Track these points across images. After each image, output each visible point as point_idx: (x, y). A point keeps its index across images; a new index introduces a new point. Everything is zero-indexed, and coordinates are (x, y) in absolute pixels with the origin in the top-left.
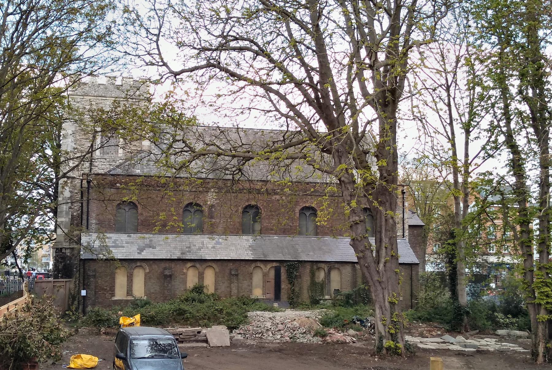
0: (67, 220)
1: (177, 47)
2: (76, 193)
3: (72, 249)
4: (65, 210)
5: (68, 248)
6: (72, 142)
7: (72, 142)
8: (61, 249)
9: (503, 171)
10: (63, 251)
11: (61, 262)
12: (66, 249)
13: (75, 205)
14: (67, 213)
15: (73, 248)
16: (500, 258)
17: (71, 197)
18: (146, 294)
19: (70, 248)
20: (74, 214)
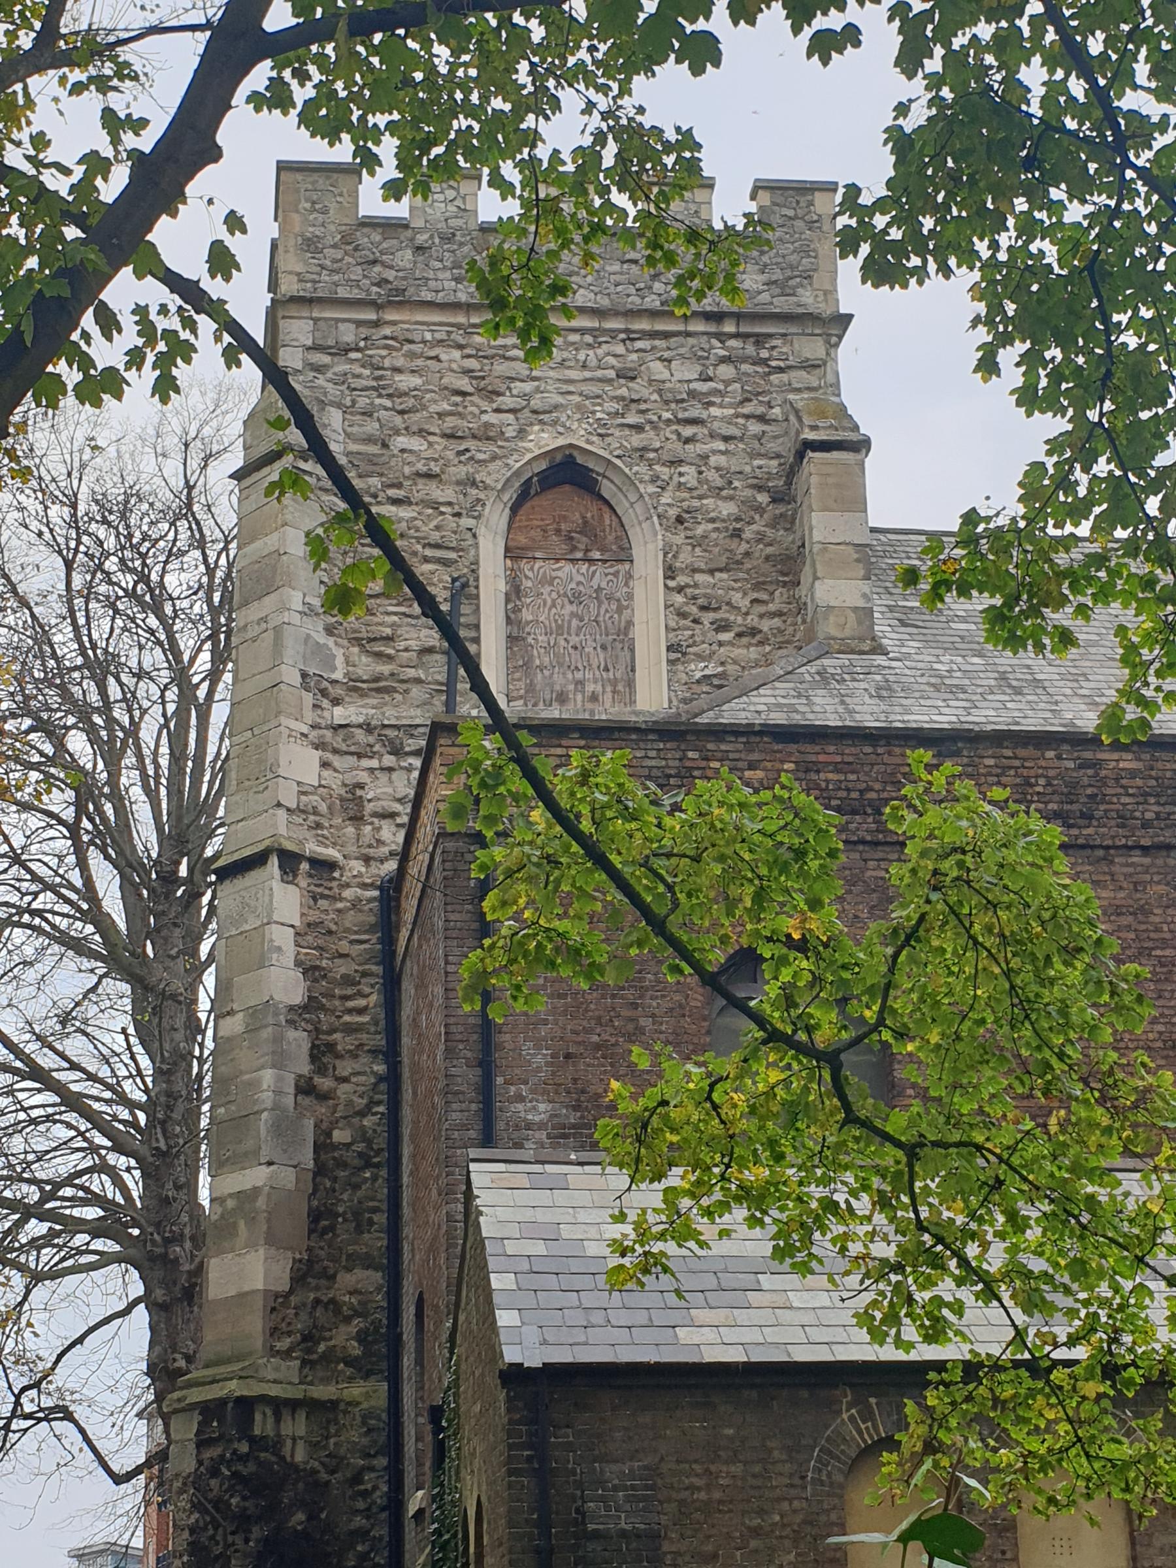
0: (287, 1178)
1: (556, 118)
2: (347, 980)
3: (324, 1412)
4: (267, 1098)
5: (294, 1405)
6: (308, 612)
7: (308, 612)
8: (245, 1405)
9: (1108, 468)
10: (262, 1424)
11: (243, 1522)
12: (278, 1406)
13: (345, 1067)
14: (283, 1128)
15: (332, 1406)
16: (550, 253)
17: (311, 1005)
18: (296, 15)
19: (313, 1406)
20: (340, 1136)
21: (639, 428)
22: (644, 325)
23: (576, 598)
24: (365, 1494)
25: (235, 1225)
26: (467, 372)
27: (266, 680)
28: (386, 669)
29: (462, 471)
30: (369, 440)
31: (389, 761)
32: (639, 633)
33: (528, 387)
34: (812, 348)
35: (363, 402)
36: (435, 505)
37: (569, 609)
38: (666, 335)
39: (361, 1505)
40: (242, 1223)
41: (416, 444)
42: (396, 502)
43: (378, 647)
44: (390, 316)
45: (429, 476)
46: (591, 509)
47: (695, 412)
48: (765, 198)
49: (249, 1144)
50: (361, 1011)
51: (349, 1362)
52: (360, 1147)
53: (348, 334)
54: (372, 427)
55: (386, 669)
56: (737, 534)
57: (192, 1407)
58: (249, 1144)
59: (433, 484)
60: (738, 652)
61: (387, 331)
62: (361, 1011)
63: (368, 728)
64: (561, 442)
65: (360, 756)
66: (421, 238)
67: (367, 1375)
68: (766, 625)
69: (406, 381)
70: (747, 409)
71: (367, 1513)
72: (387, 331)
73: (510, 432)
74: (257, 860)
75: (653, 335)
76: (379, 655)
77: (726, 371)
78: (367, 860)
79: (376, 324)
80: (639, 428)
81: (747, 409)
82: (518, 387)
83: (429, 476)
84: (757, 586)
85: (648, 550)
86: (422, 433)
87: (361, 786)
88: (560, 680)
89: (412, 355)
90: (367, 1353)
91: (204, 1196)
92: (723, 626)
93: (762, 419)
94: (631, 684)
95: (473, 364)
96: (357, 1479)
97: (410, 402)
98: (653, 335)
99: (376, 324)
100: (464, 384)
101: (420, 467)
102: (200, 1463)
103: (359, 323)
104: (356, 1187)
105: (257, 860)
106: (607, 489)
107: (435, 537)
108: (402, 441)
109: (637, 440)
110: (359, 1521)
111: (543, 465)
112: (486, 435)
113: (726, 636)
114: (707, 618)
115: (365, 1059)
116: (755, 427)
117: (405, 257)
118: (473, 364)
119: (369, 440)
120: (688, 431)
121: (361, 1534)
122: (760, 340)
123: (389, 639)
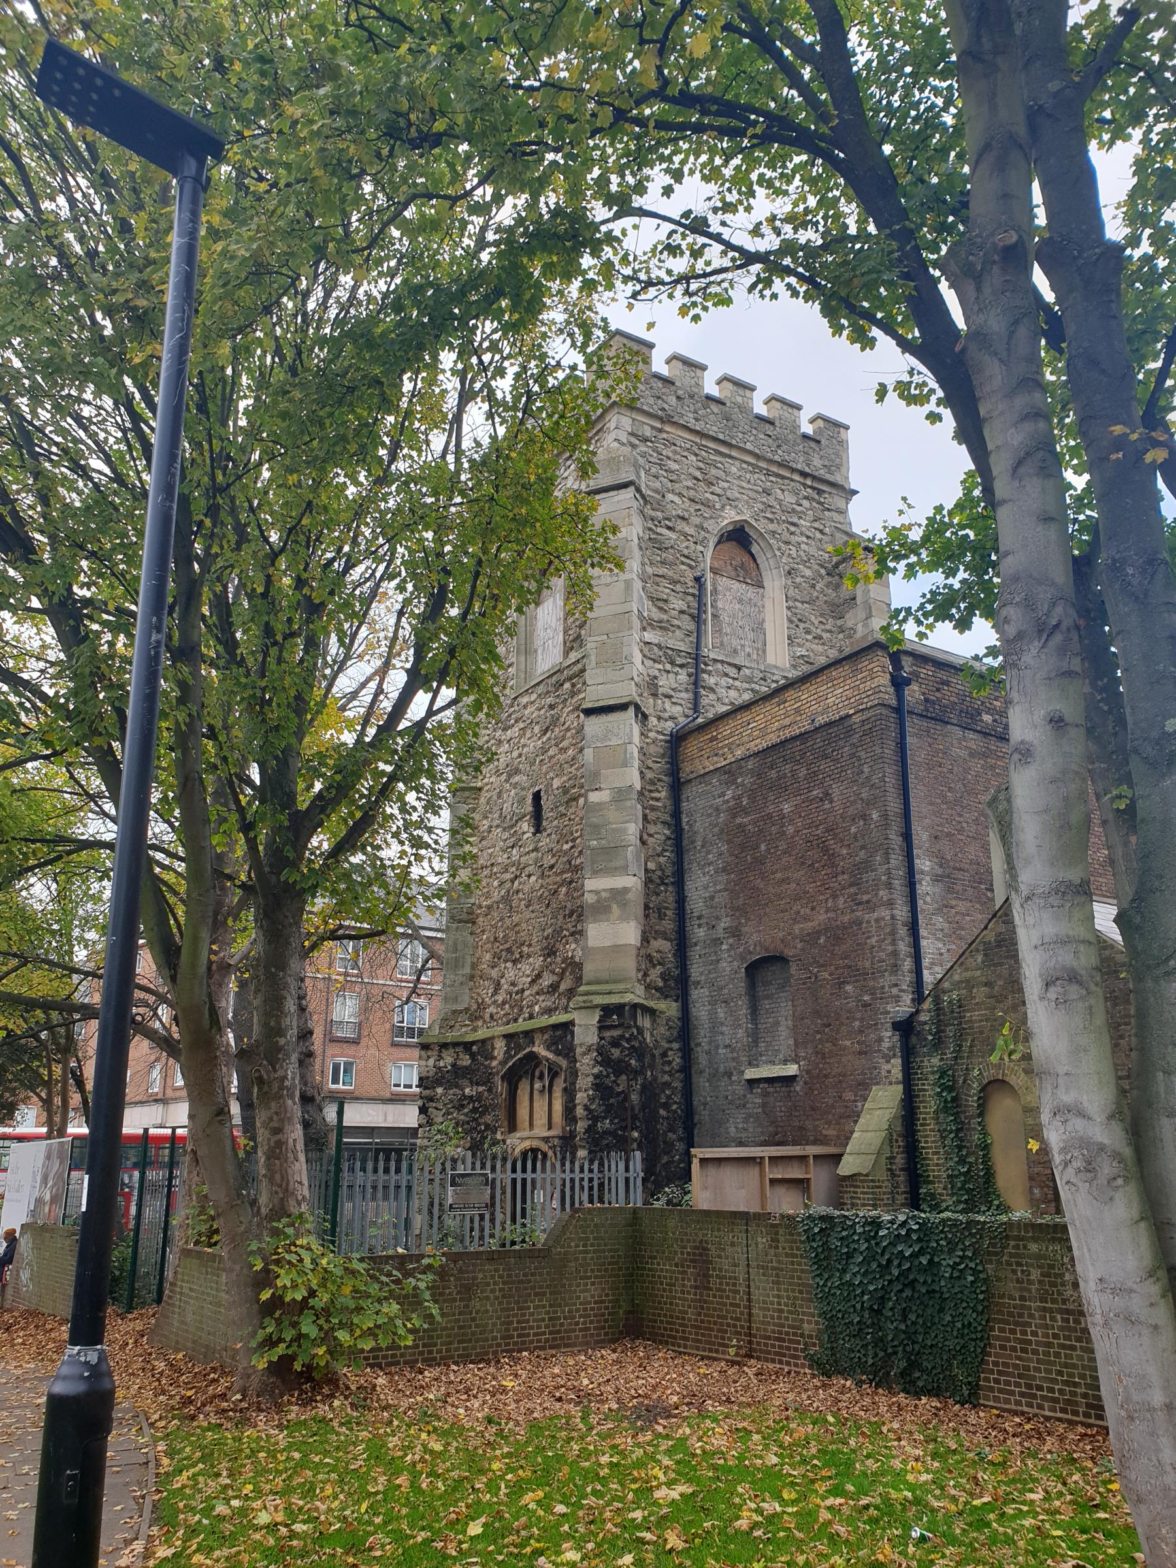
21: (771, 521)
22: (774, 469)
23: (740, 601)
24: (670, 1063)
25: (609, 907)
26: (700, 469)
27: (620, 609)
28: (665, 617)
29: (697, 521)
30: (656, 491)
31: (668, 667)
32: (769, 627)
33: (726, 485)
34: (839, 502)
35: (653, 470)
36: (686, 535)
37: (738, 606)
38: (783, 477)
39: (667, 1068)
40: (615, 906)
41: (676, 499)
42: (669, 528)
43: (661, 604)
44: (667, 428)
45: (683, 518)
46: (746, 558)
47: (795, 520)
48: (820, 423)
49: (619, 863)
50: (657, 800)
51: (657, 989)
52: (659, 873)
53: (648, 432)
54: (657, 485)
55: (665, 617)
56: (813, 586)
57: (596, 1006)
58: (619, 863)
59: (684, 524)
60: (814, 646)
61: (665, 436)
62: (657, 800)
63: (659, 646)
64: (738, 518)
65: (655, 661)
66: (680, 392)
67: (666, 997)
68: (825, 635)
69: (674, 466)
70: (816, 525)
71: (670, 1073)
72: (665, 436)
73: (718, 506)
74: (623, 707)
75: (778, 475)
76: (660, 609)
77: (806, 503)
78: (659, 718)
79: (661, 431)
80: (771, 521)
81: (816, 525)
82: (722, 484)
83: (683, 518)
84: (822, 615)
85: (774, 584)
86: (680, 495)
87: (656, 678)
88: (735, 643)
89: (675, 452)
90: (666, 986)
91: (231, 1035)
92: (808, 632)
93: (821, 532)
94: (764, 651)
95: (701, 465)
96: (664, 1054)
97: (674, 477)
98: (778, 475)
99: (661, 431)
100: (698, 474)
101: (680, 512)
102: (601, 1038)
103: (653, 428)
104: (658, 894)
105: (623, 707)
106: (755, 549)
107: (686, 552)
108: (670, 497)
109: (771, 527)
110: (667, 1078)
111: (730, 528)
112: (707, 504)
113: (810, 637)
114: (802, 625)
115: (660, 826)
116: (818, 535)
117: (673, 400)
118: (701, 465)
119: (656, 491)
120: (793, 529)
121: (667, 1085)
122: (820, 492)
123: (666, 601)
